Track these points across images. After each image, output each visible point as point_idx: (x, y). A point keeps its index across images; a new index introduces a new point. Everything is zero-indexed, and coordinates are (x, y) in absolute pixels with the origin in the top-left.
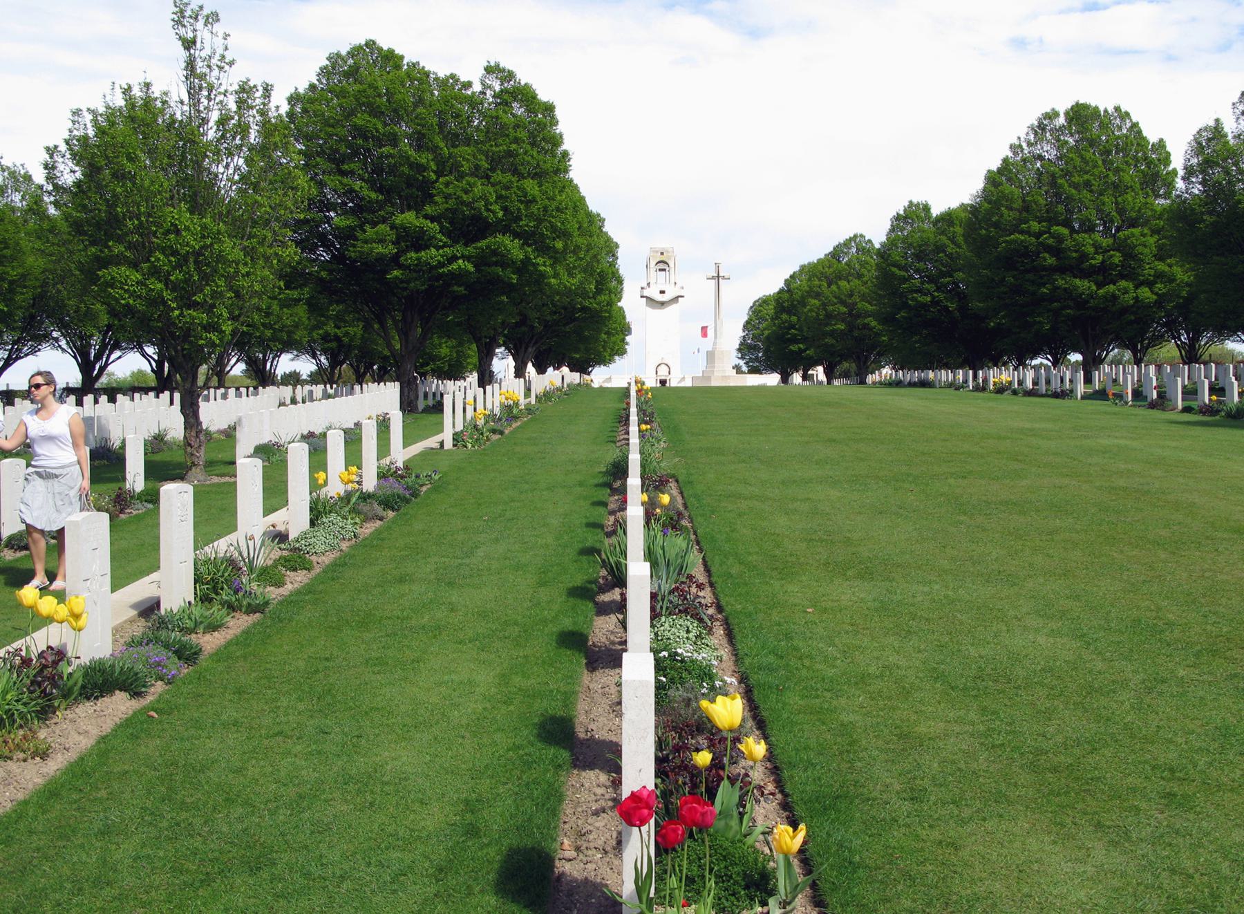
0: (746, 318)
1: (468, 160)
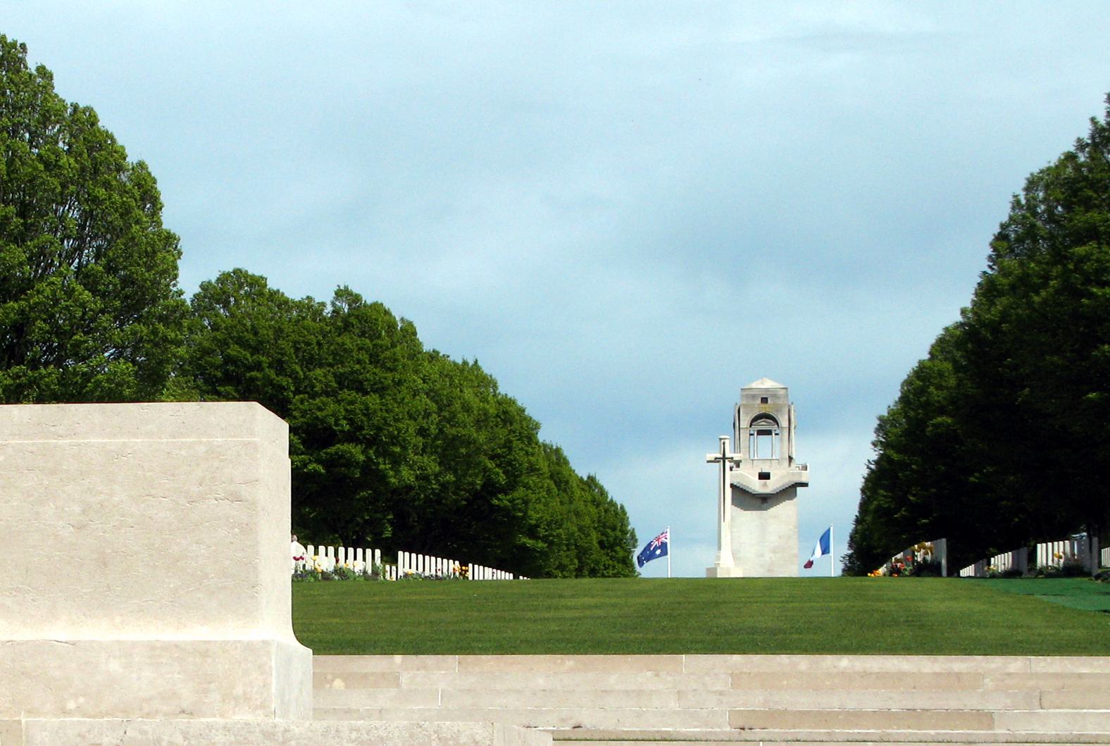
1: (320, 381)
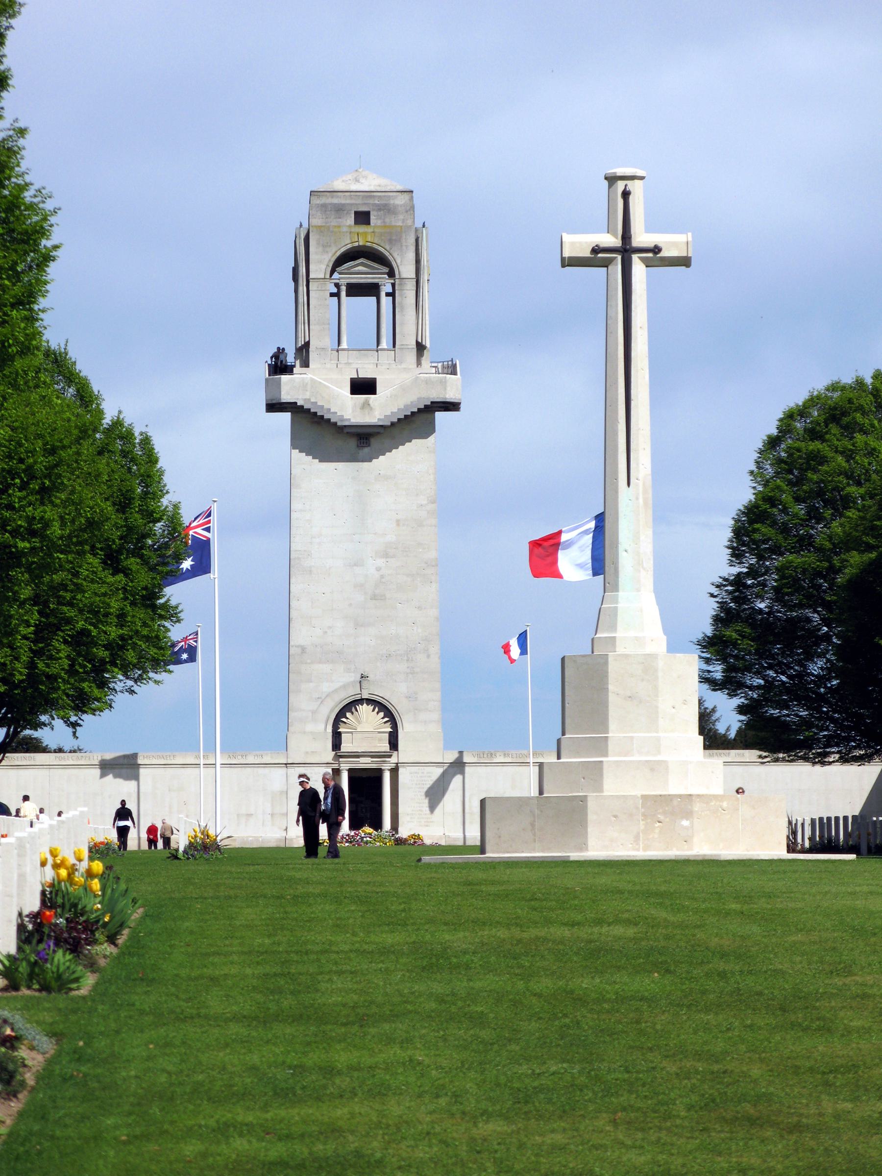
0: (744, 493)
